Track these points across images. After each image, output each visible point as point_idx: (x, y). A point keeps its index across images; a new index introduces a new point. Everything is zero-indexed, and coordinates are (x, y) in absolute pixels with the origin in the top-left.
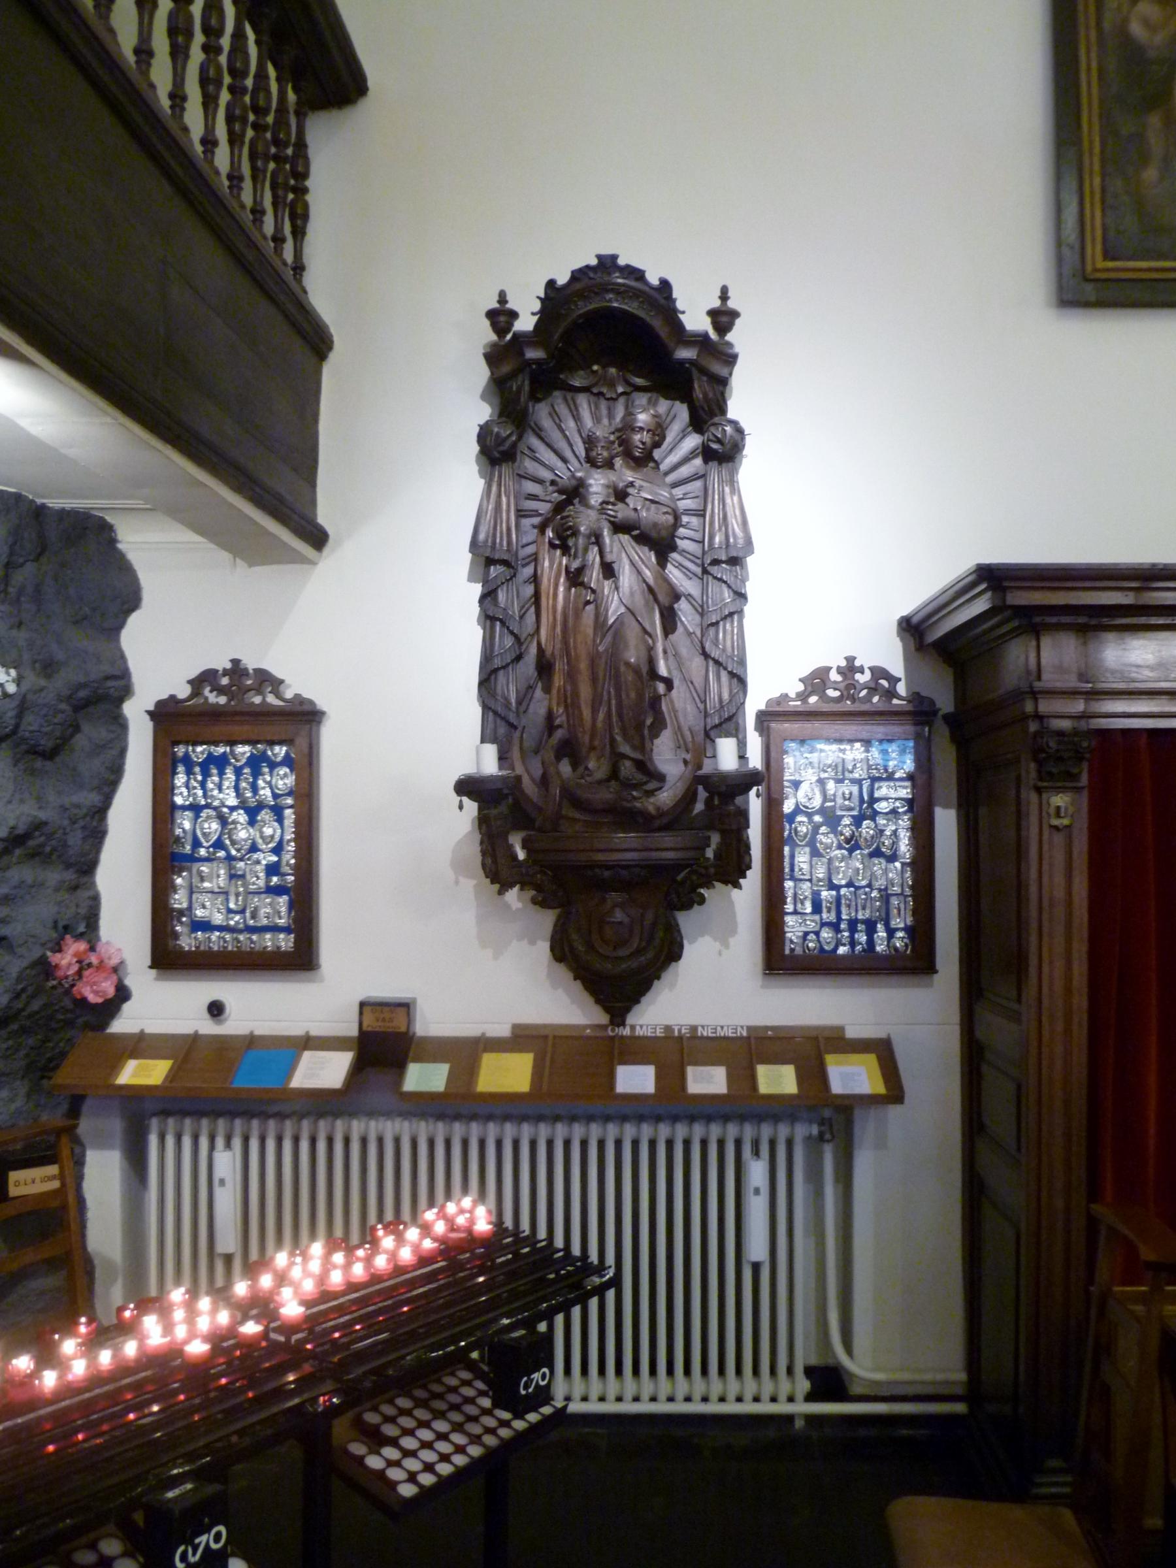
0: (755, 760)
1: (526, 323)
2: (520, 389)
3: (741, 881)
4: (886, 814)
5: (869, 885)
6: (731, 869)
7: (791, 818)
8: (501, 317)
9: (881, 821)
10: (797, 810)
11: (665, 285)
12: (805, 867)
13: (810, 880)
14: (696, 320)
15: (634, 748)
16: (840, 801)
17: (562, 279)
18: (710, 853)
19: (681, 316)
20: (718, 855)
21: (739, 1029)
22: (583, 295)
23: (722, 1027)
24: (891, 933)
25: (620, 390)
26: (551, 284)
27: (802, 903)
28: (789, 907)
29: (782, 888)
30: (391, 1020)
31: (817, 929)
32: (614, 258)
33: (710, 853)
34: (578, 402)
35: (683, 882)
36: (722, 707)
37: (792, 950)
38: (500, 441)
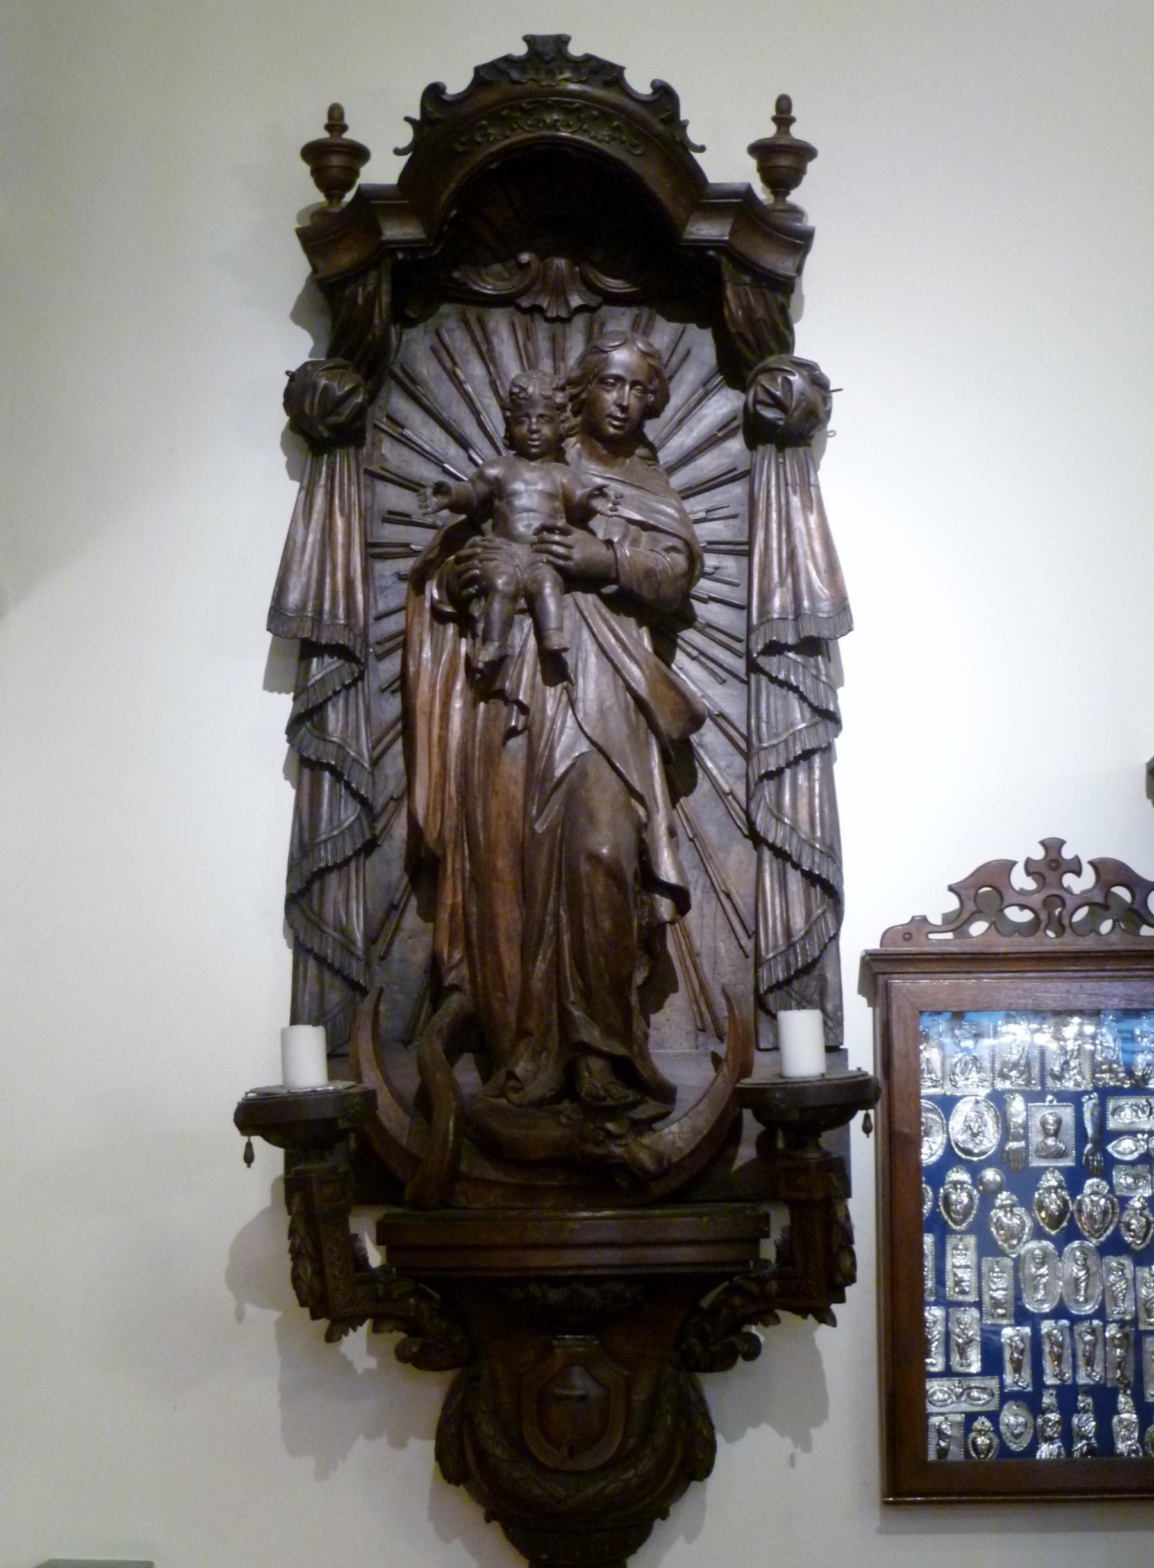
0: (861, 1055)
1: (383, 170)
2: (371, 299)
3: (835, 1308)
4: (1133, 1163)
5: (1100, 1314)
6: (815, 1285)
10: (951, 1157)
11: (664, 95)
12: (966, 1275)
13: (978, 1305)
14: (727, 163)
15: (609, 1032)
16: (1036, 1138)
17: (457, 83)
18: (768, 1250)
19: (697, 156)
22: (496, 115)
26: (434, 93)
27: (963, 1353)
28: (935, 1362)
31: (993, 1407)
32: (562, 41)
33: (768, 1250)
34: (491, 325)
36: (791, 945)
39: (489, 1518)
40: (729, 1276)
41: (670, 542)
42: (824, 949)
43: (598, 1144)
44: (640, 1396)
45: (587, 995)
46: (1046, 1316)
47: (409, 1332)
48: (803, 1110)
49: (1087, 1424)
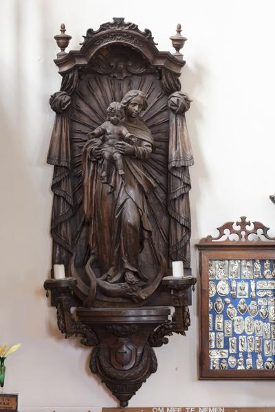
0: (194, 273)
2: (73, 77)
4: (263, 297)
5: (254, 334)
6: (181, 326)
7: (214, 299)
8: (63, 41)
9: (259, 301)
10: (217, 295)
11: (148, 32)
12: (221, 325)
13: (223, 332)
14: (164, 44)
15: (133, 266)
16: (239, 291)
17: (96, 28)
18: (170, 318)
20: (174, 318)
21: (220, 409)
22: (105, 37)
23: (212, 408)
24: (265, 359)
25: (125, 75)
26: (90, 31)
27: (219, 344)
28: (213, 345)
29: (208, 336)
30: (8, 404)
31: (227, 357)
33: (170, 318)
34: (103, 80)
35: (157, 332)
36: (177, 243)
37: (214, 368)
38: (62, 105)
39: (102, 382)
40: (161, 324)
41: (146, 143)
42: (186, 245)
43: (131, 292)
44: (139, 352)
45: (126, 250)
46: (240, 335)
47: (84, 337)
48: (178, 285)
49: (249, 361)
